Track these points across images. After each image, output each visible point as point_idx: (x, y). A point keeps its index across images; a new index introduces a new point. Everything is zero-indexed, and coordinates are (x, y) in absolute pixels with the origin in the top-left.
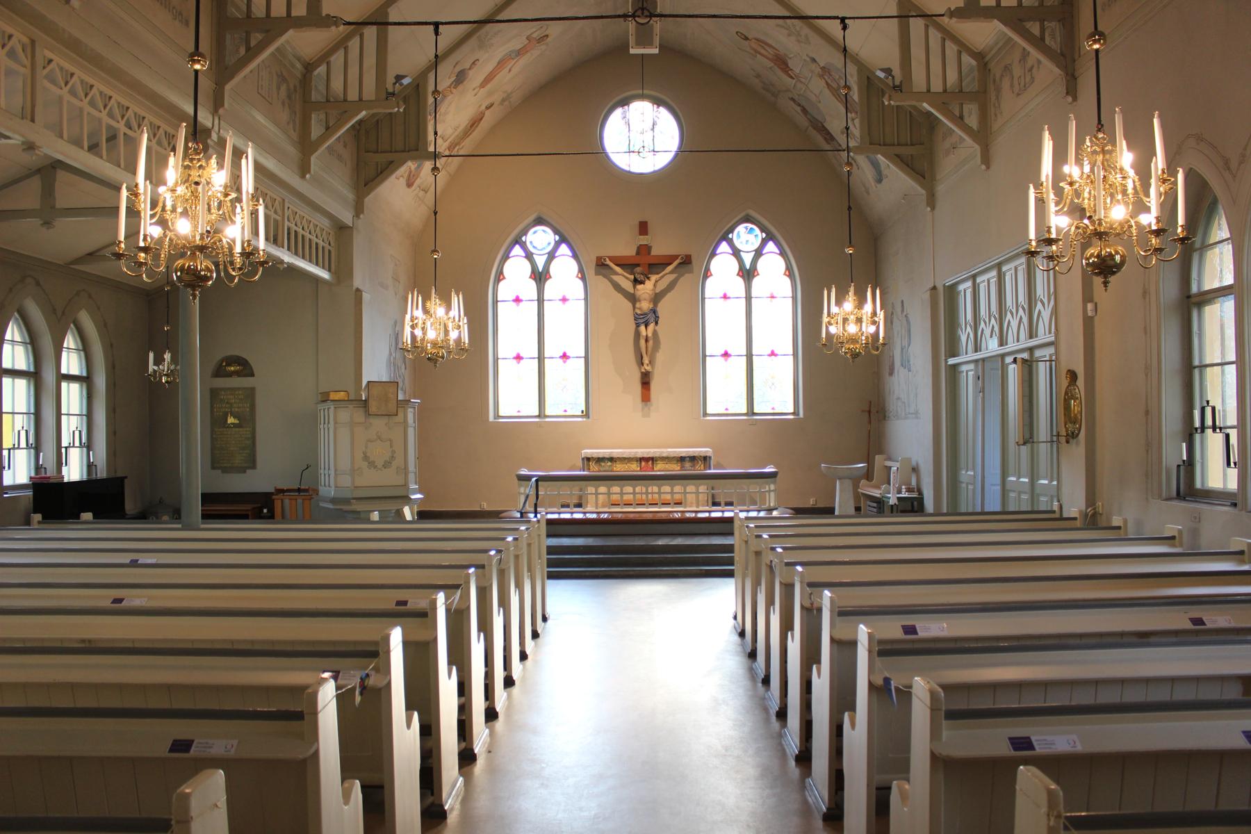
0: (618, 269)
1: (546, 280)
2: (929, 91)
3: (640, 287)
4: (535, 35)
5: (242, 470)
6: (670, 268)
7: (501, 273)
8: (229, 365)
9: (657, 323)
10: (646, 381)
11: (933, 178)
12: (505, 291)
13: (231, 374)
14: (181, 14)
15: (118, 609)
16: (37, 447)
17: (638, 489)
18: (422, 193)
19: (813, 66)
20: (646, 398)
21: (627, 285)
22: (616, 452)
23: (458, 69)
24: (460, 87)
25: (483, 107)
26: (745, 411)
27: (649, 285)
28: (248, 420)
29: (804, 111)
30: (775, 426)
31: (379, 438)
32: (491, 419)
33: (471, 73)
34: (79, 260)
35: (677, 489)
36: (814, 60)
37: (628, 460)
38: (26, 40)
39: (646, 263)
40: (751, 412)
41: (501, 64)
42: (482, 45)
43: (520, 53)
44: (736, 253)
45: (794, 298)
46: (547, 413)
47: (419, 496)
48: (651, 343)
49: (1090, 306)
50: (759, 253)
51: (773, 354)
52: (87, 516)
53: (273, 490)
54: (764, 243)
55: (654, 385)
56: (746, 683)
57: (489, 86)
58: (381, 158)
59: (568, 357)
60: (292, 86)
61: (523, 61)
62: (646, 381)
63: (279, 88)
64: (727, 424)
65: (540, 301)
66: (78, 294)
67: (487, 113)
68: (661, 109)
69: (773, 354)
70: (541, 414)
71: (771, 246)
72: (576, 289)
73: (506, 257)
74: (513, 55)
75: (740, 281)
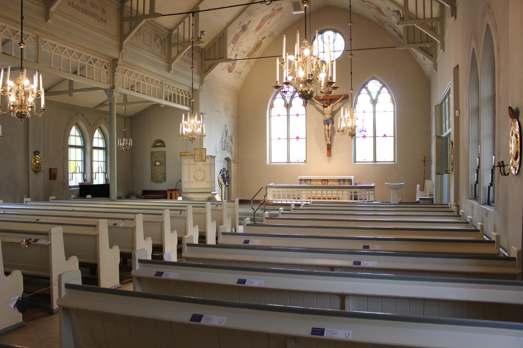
0: (317, 102)
1: (290, 107)
2: (424, 18)
3: (326, 109)
4: (276, 8)
5: (161, 182)
6: (339, 100)
7: (273, 105)
8: (157, 143)
9: (333, 124)
10: (329, 148)
11: (436, 57)
12: (274, 111)
13: (158, 147)
14: (102, 19)
15: (37, 222)
16: (84, 173)
17: (334, 192)
18: (238, 75)
19: (390, 11)
20: (329, 154)
21: (321, 108)
22: (312, 177)
23: (242, 25)
24: (245, 32)
25: (261, 39)
26: (372, 160)
27: (329, 108)
28: (163, 163)
29: (394, 30)
30: (386, 167)
32: (268, 163)
33: (249, 26)
34: (98, 106)
35: (334, 192)
36: (389, 8)
37: (317, 180)
38: (35, 36)
39: (327, 99)
40: (375, 161)
41: (263, 21)
42: (250, 14)
43: (271, 16)
44: (369, 93)
45: (394, 112)
46: (291, 161)
48: (330, 132)
49: (457, 112)
50: (379, 93)
51: (385, 136)
52: (89, 196)
53: (167, 189)
54: (381, 88)
55: (333, 150)
57: (260, 31)
58: (210, 62)
59: (299, 138)
60: (163, 39)
61: (274, 19)
62: (329, 148)
63: (155, 40)
64: (365, 166)
65: (288, 116)
66: (100, 118)
67: (263, 41)
68: (337, 34)
69: (385, 136)
70: (289, 162)
71: (384, 89)
72: (302, 110)
73: (275, 98)
74: (268, 17)
75: (285, 109)
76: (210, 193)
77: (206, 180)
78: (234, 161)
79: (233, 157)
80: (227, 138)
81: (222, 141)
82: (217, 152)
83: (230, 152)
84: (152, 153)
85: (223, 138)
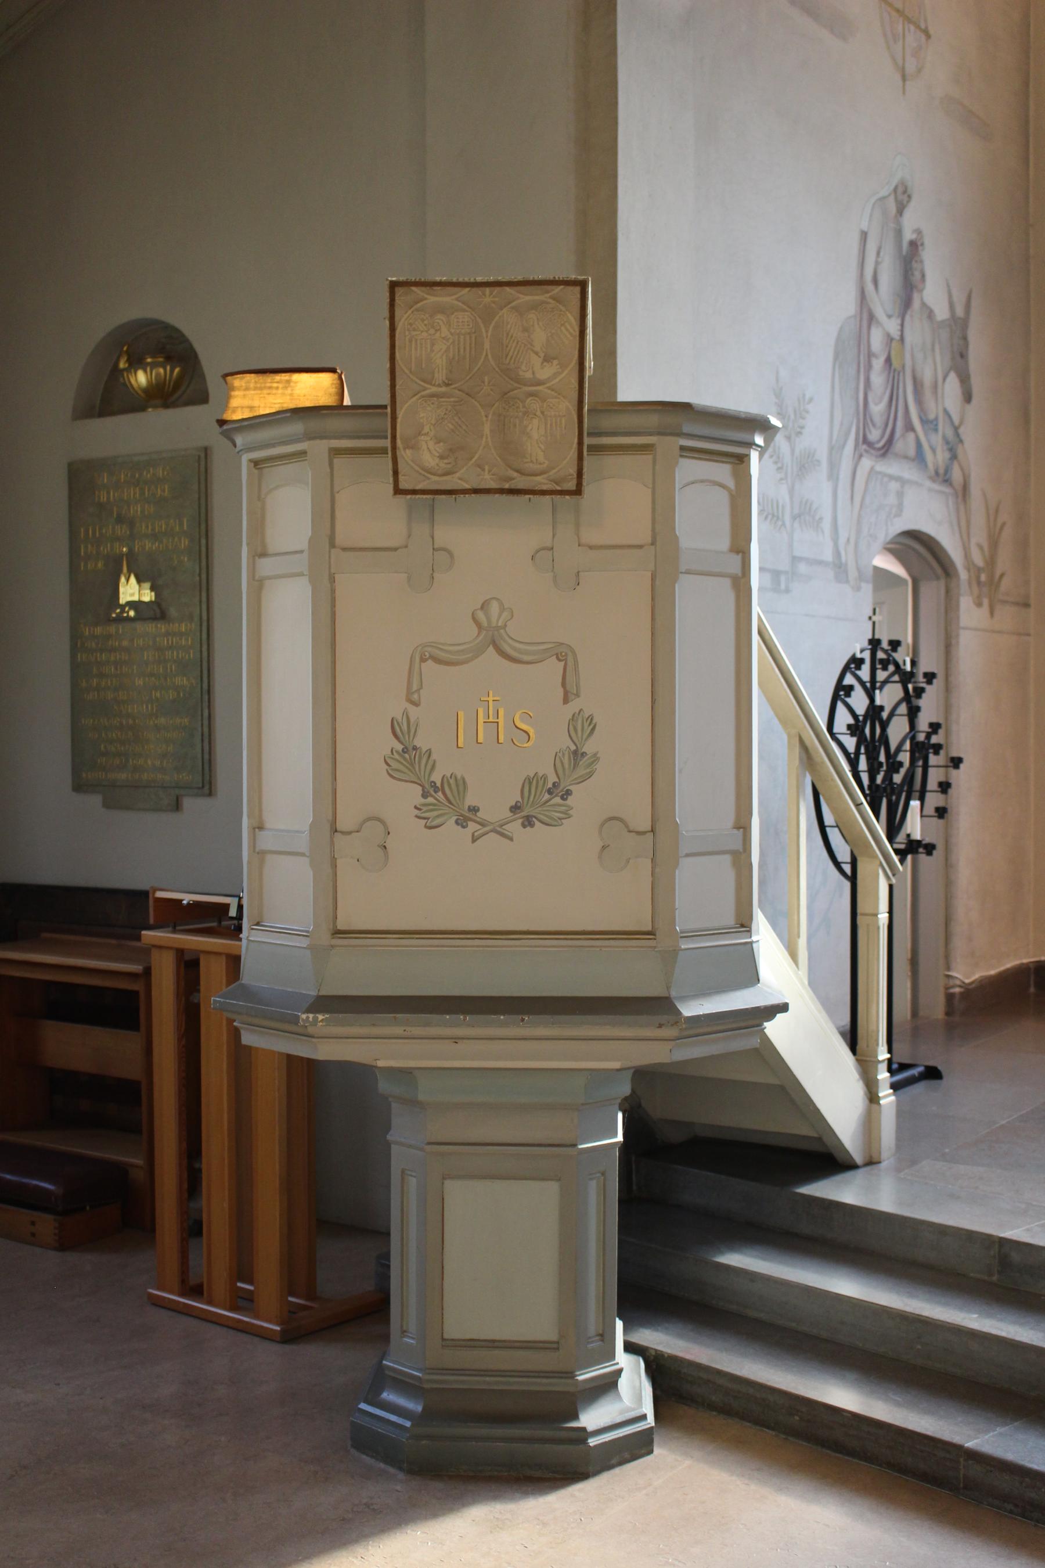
31: (493, 640)
47: (177, 370)
56: (954, 728)
77: (587, 800)
78: (988, 584)
79: (979, 536)
80: (916, 333)
81: (854, 348)
83: (943, 477)
84: (81, 478)
85: (867, 317)
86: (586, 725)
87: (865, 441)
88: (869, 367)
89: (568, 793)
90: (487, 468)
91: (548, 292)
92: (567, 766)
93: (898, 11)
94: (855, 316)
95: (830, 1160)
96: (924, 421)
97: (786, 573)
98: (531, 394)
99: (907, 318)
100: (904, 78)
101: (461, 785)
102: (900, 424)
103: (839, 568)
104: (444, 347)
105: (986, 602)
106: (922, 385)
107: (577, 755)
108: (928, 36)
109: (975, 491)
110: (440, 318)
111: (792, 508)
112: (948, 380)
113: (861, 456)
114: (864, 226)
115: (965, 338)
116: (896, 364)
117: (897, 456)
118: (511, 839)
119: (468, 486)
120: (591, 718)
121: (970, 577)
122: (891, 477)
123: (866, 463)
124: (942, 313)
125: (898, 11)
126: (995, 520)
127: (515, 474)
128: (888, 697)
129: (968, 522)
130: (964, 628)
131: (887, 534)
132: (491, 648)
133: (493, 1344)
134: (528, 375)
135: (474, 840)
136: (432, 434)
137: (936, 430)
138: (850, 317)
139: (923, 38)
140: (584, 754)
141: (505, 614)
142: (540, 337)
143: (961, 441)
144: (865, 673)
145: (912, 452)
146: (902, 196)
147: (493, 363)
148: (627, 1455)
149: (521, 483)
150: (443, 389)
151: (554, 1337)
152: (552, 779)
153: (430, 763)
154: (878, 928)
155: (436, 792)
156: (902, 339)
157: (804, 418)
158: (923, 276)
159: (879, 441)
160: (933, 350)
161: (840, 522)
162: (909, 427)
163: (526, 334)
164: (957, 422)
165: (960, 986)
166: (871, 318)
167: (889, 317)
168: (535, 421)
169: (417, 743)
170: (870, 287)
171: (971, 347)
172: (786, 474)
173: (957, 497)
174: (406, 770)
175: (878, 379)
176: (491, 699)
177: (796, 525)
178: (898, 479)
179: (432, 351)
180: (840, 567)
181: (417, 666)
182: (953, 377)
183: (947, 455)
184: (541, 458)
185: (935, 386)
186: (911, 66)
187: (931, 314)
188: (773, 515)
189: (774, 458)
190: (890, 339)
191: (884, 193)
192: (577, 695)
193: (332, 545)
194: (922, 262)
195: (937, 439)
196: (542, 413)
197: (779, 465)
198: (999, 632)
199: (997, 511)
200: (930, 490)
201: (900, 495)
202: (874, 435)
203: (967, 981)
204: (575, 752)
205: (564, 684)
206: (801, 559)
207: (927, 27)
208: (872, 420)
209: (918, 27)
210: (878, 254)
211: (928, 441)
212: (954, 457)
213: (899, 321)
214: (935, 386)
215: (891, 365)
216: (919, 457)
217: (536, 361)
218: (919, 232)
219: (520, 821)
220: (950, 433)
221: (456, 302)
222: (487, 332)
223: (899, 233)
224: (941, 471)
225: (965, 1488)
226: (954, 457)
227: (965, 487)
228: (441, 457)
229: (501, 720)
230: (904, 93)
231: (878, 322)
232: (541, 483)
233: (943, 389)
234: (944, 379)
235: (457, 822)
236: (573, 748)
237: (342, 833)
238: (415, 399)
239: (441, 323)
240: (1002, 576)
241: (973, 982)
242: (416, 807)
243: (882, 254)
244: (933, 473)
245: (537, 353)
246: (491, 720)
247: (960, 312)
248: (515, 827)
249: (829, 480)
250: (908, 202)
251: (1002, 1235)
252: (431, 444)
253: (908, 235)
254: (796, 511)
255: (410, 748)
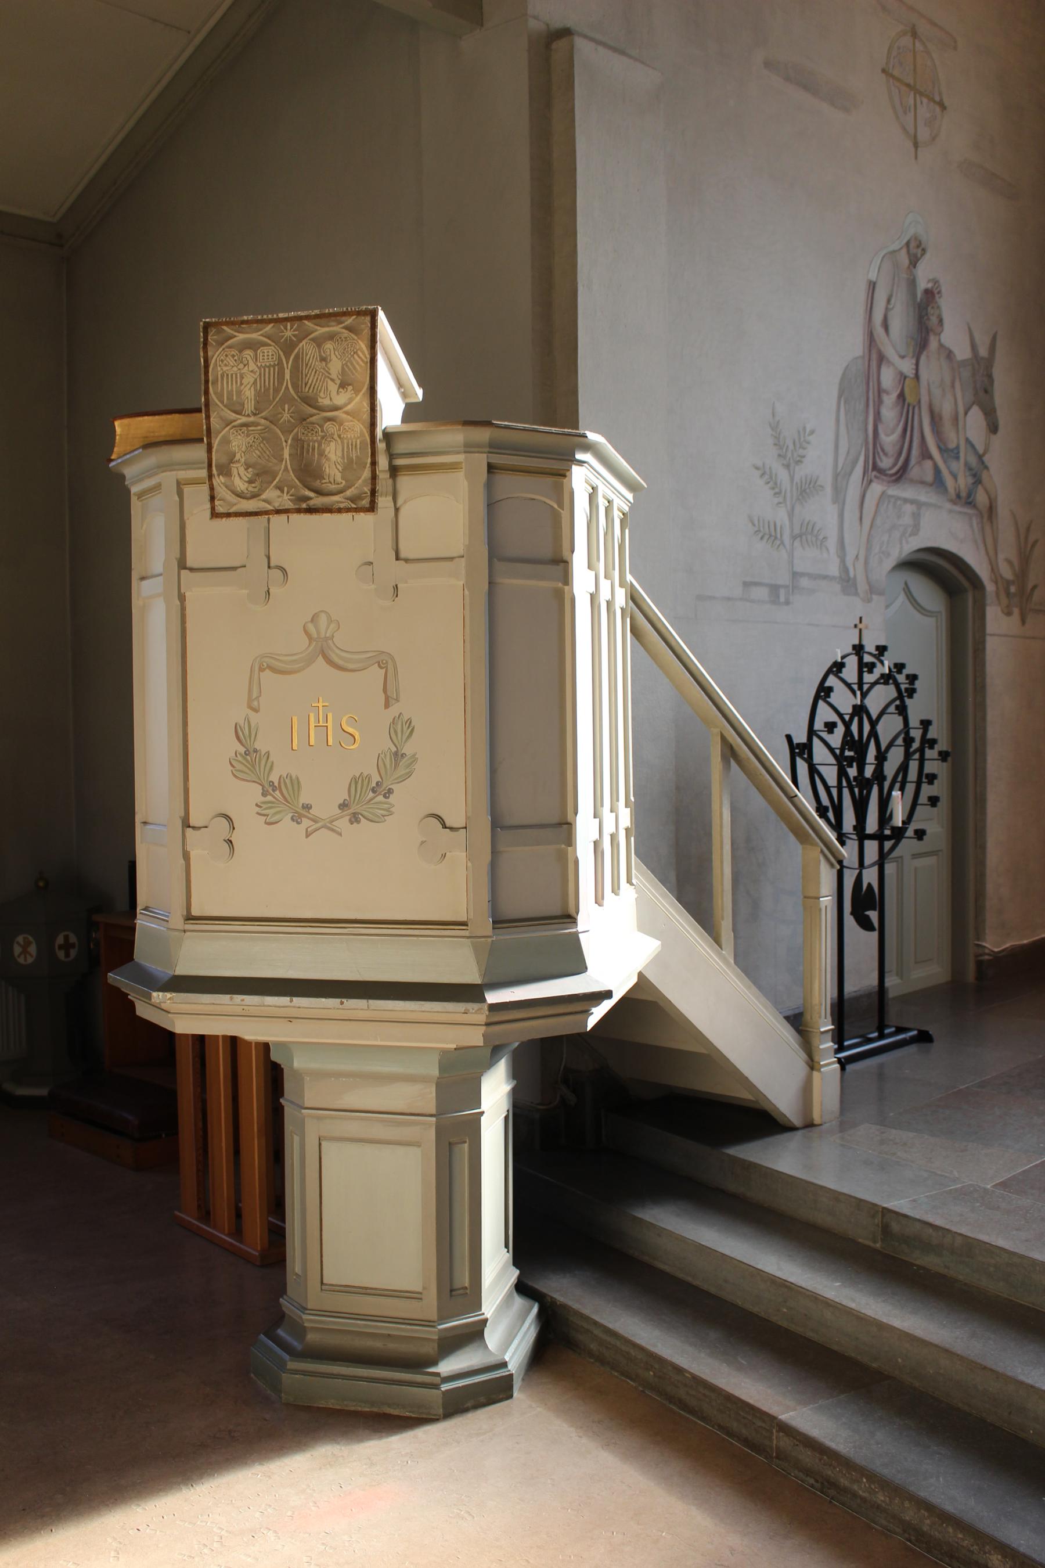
31: (323, 650)
76: (470, 993)
77: (409, 799)
78: (1021, 596)
79: (1007, 551)
81: (863, 385)
82: (807, 490)
83: (966, 500)
85: (874, 354)
86: (405, 728)
87: (875, 467)
88: (880, 402)
89: (390, 791)
90: (286, 489)
91: (342, 323)
92: (388, 767)
93: (908, 85)
94: (863, 357)
95: (760, 1121)
96: (943, 450)
97: (786, 587)
98: (330, 419)
99: (923, 358)
100: (916, 145)
101: (295, 784)
102: (915, 452)
103: (848, 583)
104: (252, 380)
105: (1016, 611)
106: (941, 418)
107: (398, 756)
108: (943, 107)
109: (1003, 512)
110: (248, 353)
111: (792, 530)
112: (970, 414)
113: (871, 481)
114: (873, 276)
115: (990, 377)
116: (910, 399)
117: (912, 481)
118: (340, 835)
119: (270, 507)
120: (409, 722)
121: (997, 588)
122: (906, 501)
123: (877, 488)
124: (963, 352)
125: (908, 85)
126: (1026, 538)
127: (312, 494)
128: (878, 698)
129: (995, 541)
130: (991, 635)
131: (901, 552)
132: (320, 658)
133: (366, 1291)
134: (326, 402)
135: (307, 836)
136: (243, 460)
137: (957, 458)
138: (857, 358)
139: (938, 109)
140: (403, 755)
141: (332, 626)
142: (335, 366)
143: (986, 468)
144: (850, 673)
145: (929, 477)
146: (915, 251)
147: (292, 392)
148: (482, 1399)
149: (318, 501)
150: (252, 419)
151: (418, 1288)
152: (375, 778)
153: (269, 764)
154: (820, 910)
155: (274, 791)
156: (917, 376)
157: (804, 449)
158: (941, 321)
159: (890, 469)
160: (953, 386)
161: (847, 541)
162: (926, 455)
163: (324, 363)
164: (981, 450)
165: (988, 954)
166: (881, 358)
167: (903, 357)
168: (333, 444)
169: (257, 746)
170: (879, 330)
171: (996, 383)
172: (785, 497)
173: (982, 517)
174: (248, 771)
175: (889, 413)
176: (320, 705)
177: (797, 543)
178: (912, 502)
179: (241, 384)
180: (848, 581)
181: (256, 676)
182: (976, 413)
183: (970, 480)
184: (339, 479)
185: (956, 420)
186: (923, 134)
187: (950, 355)
188: (771, 536)
189: (771, 484)
190: (903, 377)
191: (895, 246)
192: (397, 700)
193: (182, 565)
194: (939, 307)
195: (958, 466)
196: (339, 436)
197: (777, 490)
198: (1033, 638)
199: (1028, 529)
200: (950, 511)
201: (916, 516)
202: (885, 463)
203: (996, 950)
204: (396, 754)
205: (385, 690)
206: (802, 575)
207: (941, 100)
208: (883, 450)
209: (931, 99)
210: (889, 301)
211: (948, 468)
212: (978, 481)
213: (914, 361)
214: (956, 420)
215: (904, 400)
216: (938, 482)
217: (333, 387)
218: (936, 282)
219: (348, 818)
220: (973, 461)
221: (261, 338)
222: (287, 363)
223: (912, 283)
224: (964, 494)
225: (777, 1457)
226: (978, 481)
227: (992, 509)
228: (250, 482)
229: (330, 724)
230: (916, 158)
231: (889, 362)
232: (338, 502)
233: (965, 421)
234: (966, 414)
235: (292, 819)
236: (394, 749)
237: (194, 828)
238: (227, 429)
239: (249, 358)
240: (1035, 587)
241: (1003, 951)
242: (257, 805)
243: (893, 301)
244: (954, 496)
245: (333, 380)
246: (321, 724)
247: (983, 352)
248: (343, 824)
249: (834, 502)
250: (922, 255)
251: (885, 1205)
252: (242, 470)
253: (922, 285)
254: (797, 531)
255: (251, 751)
